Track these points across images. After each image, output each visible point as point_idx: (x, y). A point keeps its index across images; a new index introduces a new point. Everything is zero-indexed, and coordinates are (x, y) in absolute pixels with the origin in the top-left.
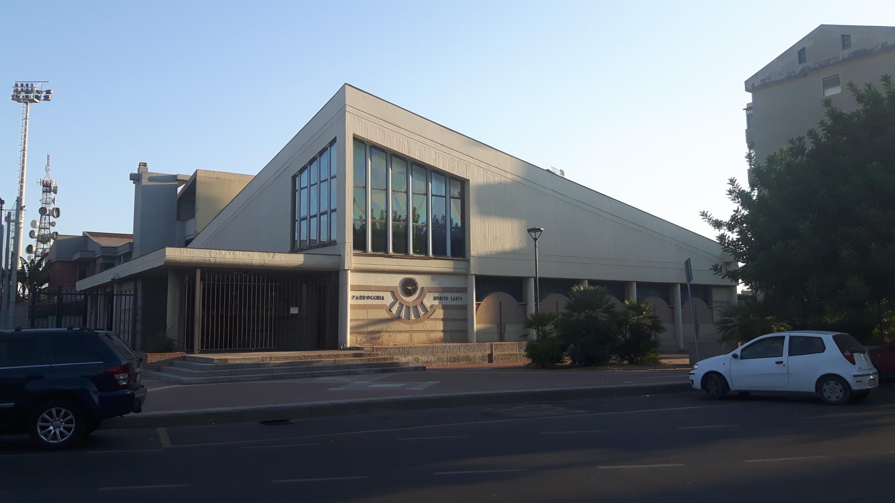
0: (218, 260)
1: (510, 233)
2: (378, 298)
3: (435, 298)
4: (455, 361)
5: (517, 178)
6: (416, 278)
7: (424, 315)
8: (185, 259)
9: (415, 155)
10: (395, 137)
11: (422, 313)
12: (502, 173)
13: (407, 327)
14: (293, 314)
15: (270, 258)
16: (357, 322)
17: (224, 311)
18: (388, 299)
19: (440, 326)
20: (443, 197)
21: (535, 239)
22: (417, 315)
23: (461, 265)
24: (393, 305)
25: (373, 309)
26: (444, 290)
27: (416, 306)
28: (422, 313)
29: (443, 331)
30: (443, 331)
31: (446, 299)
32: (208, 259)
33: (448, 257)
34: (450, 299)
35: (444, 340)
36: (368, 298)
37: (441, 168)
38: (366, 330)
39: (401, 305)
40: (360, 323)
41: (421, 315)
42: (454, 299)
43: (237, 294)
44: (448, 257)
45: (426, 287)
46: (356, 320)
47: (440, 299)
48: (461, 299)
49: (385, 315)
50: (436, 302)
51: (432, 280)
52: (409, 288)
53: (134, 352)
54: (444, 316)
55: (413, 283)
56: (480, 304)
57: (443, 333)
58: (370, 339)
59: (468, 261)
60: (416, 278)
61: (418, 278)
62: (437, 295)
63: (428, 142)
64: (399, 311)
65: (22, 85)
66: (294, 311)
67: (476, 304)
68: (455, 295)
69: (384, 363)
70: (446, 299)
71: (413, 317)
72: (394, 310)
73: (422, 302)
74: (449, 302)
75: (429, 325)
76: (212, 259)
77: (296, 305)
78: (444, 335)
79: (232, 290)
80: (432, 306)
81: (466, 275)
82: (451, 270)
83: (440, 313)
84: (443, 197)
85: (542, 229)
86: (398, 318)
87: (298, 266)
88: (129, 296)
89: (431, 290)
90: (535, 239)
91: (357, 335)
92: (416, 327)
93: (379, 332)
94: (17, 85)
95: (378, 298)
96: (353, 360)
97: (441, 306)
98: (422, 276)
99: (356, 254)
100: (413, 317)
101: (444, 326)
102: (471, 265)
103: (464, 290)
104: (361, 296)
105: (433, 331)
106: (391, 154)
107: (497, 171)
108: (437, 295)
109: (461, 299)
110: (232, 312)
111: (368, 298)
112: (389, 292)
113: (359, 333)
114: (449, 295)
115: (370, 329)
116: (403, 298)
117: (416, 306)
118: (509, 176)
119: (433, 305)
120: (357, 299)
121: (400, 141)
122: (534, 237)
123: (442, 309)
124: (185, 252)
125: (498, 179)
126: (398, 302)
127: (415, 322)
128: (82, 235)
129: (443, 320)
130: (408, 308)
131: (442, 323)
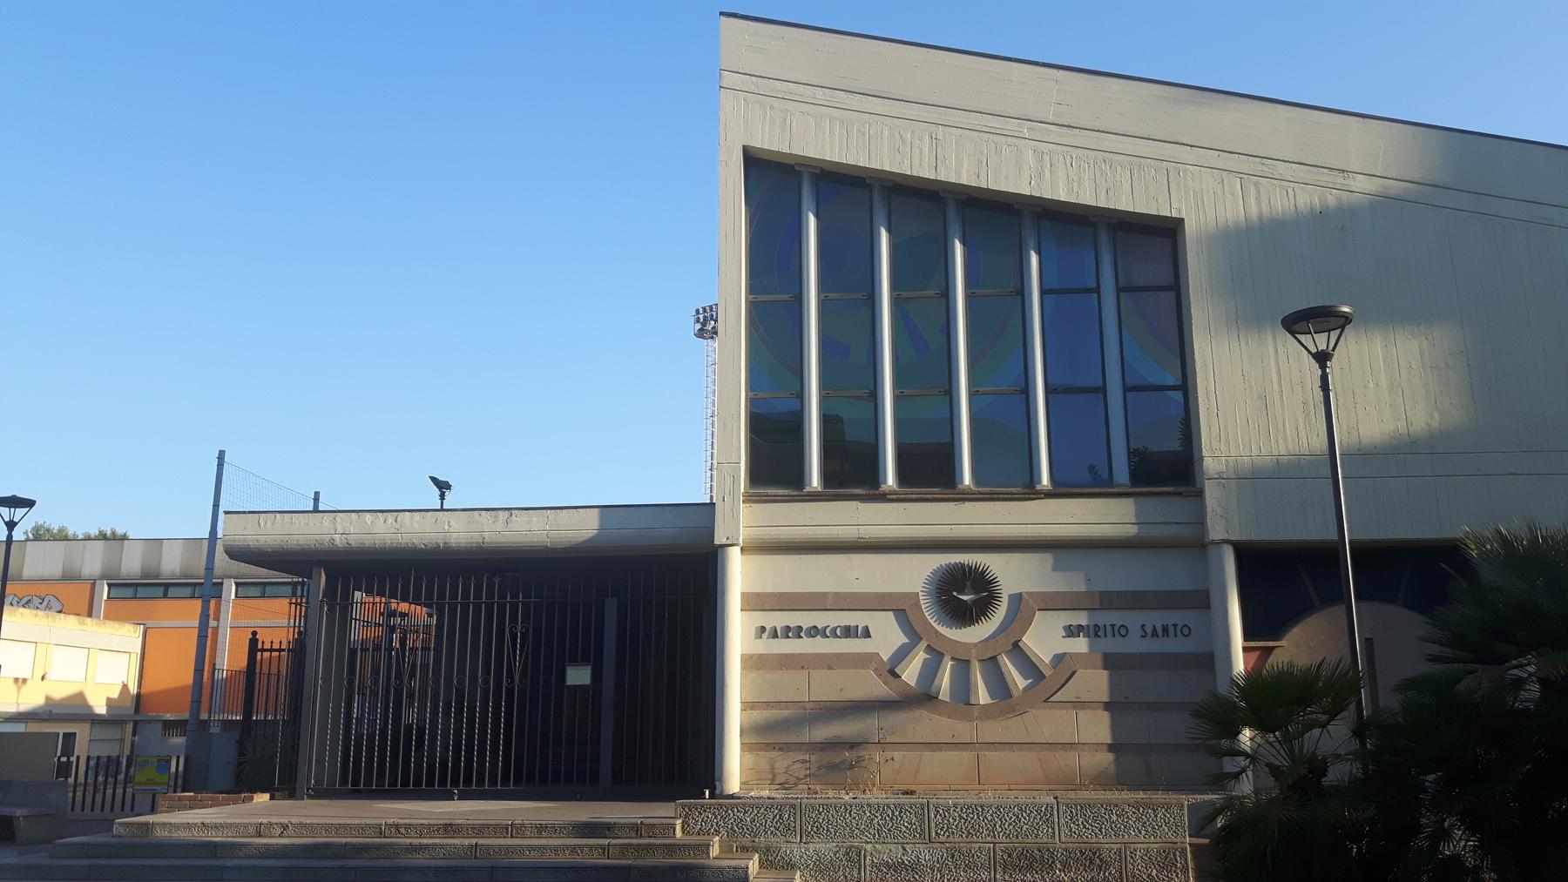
0: (354, 540)
1: (1383, 382)
2: (848, 632)
3: (1071, 632)
4: (1030, 868)
5: (1395, 187)
6: (992, 563)
7: (1027, 689)
8: (270, 542)
9: (958, 172)
10: (886, 132)
11: (1019, 681)
12: (1325, 177)
13: (964, 730)
14: (575, 687)
15: (499, 526)
16: (774, 712)
17: (553, 680)
18: (886, 636)
19: (1098, 727)
20: (1090, 291)
21: (1322, 358)
22: (999, 685)
23: (1167, 512)
24: (902, 654)
25: (830, 668)
26: (1108, 601)
27: (994, 658)
28: (1019, 681)
29: (1111, 748)
30: (1111, 748)
31: (1121, 631)
32: (327, 538)
33: (1119, 486)
34: (1135, 631)
35: (1122, 780)
36: (814, 632)
37: (1062, 195)
38: (805, 737)
39: (936, 655)
40: (784, 713)
41: (1015, 694)
42: (1155, 633)
43: (527, 630)
44: (1119, 486)
45: (1028, 593)
46: (778, 704)
47: (1094, 632)
48: (1186, 631)
49: (871, 686)
50: (1080, 645)
51: (1054, 569)
52: (965, 598)
53: (1028, 763)
54: (1112, 692)
55: (982, 583)
56: (1273, 648)
57: (1110, 757)
58: (820, 768)
59: (1200, 494)
60: (992, 563)
61: (995, 564)
62: (1082, 619)
63: (1011, 125)
64: (930, 672)
65: (704, 309)
66: (578, 676)
67: (1245, 649)
68: (1155, 619)
69: (638, 868)
70: (1121, 631)
71: (983, 696)
72: (911, 673)
73: (1016, 645)
74: (1133, 644)
75: (1047, 724)
76: (337, 537)
77: (584, 661)
78: (1116, 760)
79: (514, 620)
80: (1059, 659)
81: (1198, 546)
82: (1131, 530)
83: (1095, 683)
84: (1090, 291)
85: (1346, 309)
86: (924, 697)
87: (584, 542)
88: (265, 647)
89: (1052, 603)
90: (1322, 358)
91: (775, 754)
92: (994, 730)
93: (853, 745)
94: (698, 312)
95: (848, 632)
96: (574, 848)
97: (1099, 660)
98: (1016, 558)
99: (758, 495)
100: (983, 696)
101: (1115, 726)
102: (1209, 509)
103: (1203, 601)
104: (788, 628)
105: (1071, 746)
106: (812, 174)
107: (1301, 173)
108: (1082, 619)
109: (1186, 631)
110: (402, 681)
111: (814, 632)
112: (891, 613)
113: (785, 748)
114: (1133, 619)
115: (823, 732)
116: (940, 629)
117: (994, 658)
118: (1361, 184)
119: (1064, 654)
120: (775, 635)
121: (904, 141)
122: (1314, 350)
123: (1105, 668)
124: (269, 523)
125: (1306, 199)
126: (923, 644)
127: (987, 713)
128: (717, 542)
129: (1107, 706)
130: (963, 665)
131: (1105, 717)
